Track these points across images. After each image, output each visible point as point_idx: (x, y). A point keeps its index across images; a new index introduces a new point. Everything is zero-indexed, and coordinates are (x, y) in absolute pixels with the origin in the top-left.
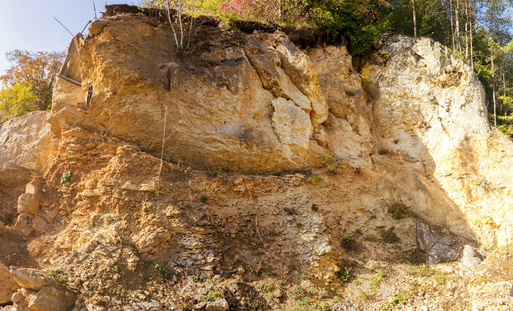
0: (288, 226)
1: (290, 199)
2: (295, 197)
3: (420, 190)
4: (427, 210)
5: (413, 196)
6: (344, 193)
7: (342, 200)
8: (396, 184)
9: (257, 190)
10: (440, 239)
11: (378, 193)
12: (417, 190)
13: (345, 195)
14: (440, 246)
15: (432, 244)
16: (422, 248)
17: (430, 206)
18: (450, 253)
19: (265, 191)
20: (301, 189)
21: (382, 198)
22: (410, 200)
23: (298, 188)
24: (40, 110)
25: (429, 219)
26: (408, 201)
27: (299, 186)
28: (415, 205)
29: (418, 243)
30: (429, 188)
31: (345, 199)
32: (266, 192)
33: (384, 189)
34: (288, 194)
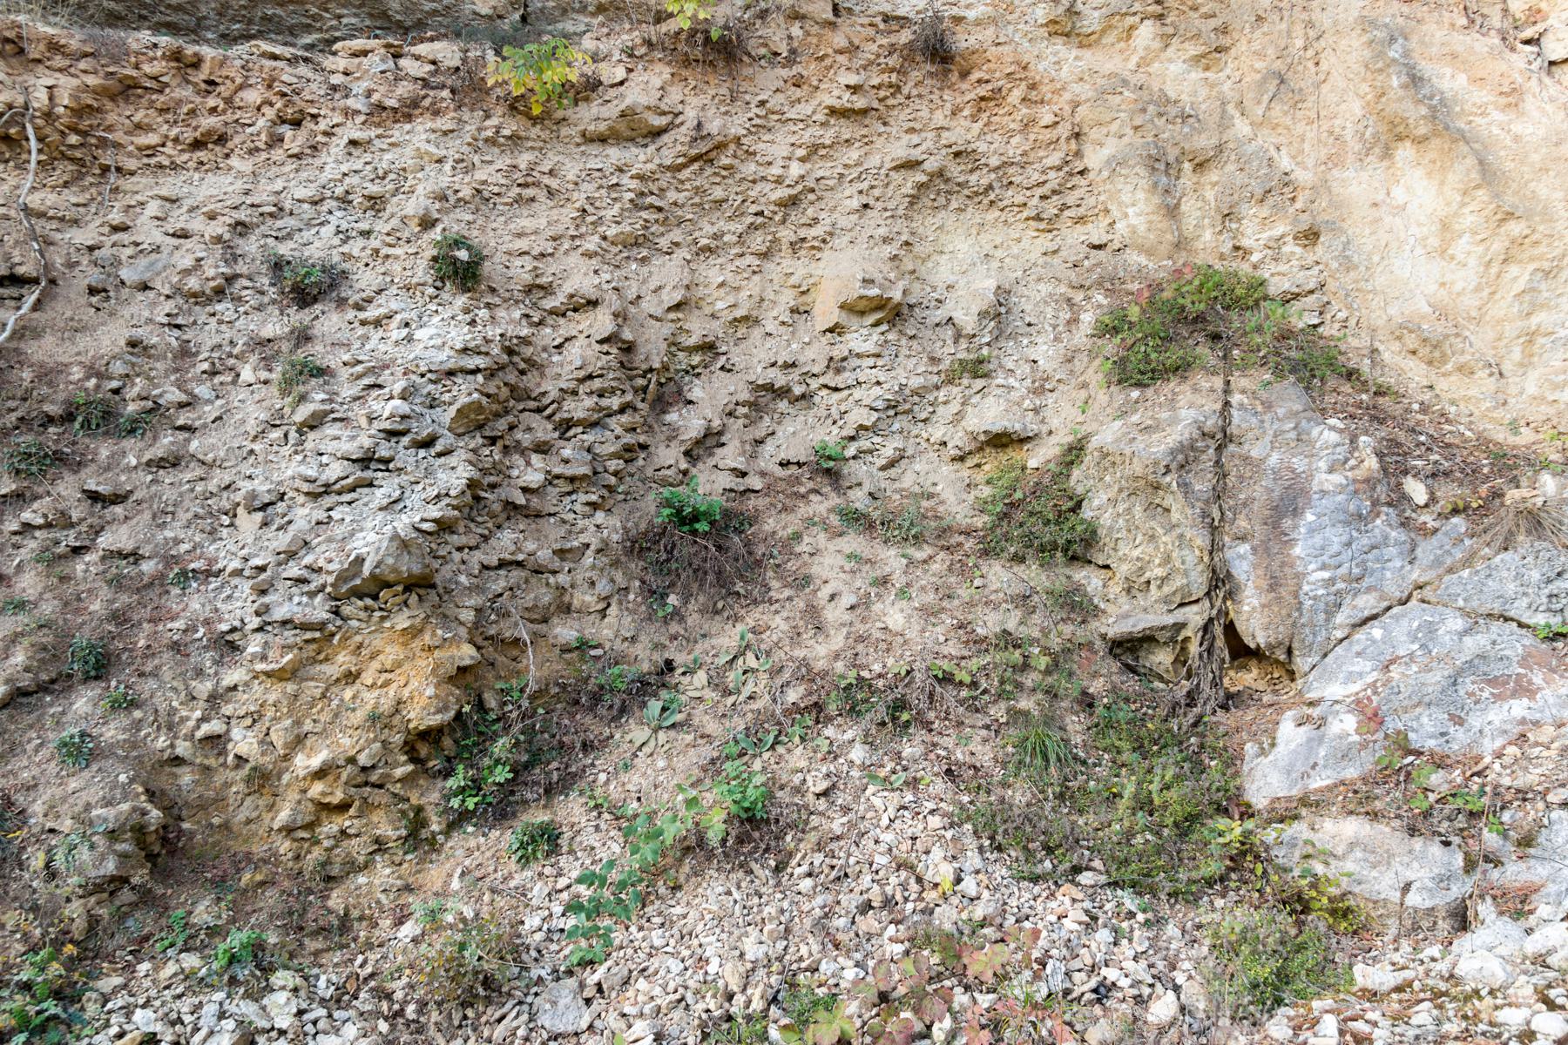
0: (247, 374)
1: (345, 201)
2: (374, 189)
3: (1405, 152)
4: (1441, 313)
5: (1336, 205)
6: (782, 193)
7: (758, 241)
8: (1224, 123)
9: (139, 127)
10: (1468, 562)
11: (1071, 199)
12: (1387, 154)
13: (793, 202)
14: (1431, 629)
15: (1367, 603)
16: (1255, 627)
17: (1465, 278)
18: (1519, 708)
19: (189, 136)
20: (418, 135)
21: (1096, 233)
22: (1310, 236)
23: (398, 132)
24: (1497, 697)
25: (1450, 387)
26: (1290, 247)
27: (407, 111)
28: (1348, 280)
29: (1220, 582)
30: (1493, 124)
31: (786, 234)
32: (197, 145)
33: (1116, 165)
34: (333, 164)
